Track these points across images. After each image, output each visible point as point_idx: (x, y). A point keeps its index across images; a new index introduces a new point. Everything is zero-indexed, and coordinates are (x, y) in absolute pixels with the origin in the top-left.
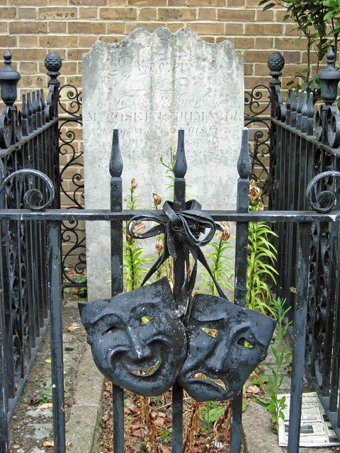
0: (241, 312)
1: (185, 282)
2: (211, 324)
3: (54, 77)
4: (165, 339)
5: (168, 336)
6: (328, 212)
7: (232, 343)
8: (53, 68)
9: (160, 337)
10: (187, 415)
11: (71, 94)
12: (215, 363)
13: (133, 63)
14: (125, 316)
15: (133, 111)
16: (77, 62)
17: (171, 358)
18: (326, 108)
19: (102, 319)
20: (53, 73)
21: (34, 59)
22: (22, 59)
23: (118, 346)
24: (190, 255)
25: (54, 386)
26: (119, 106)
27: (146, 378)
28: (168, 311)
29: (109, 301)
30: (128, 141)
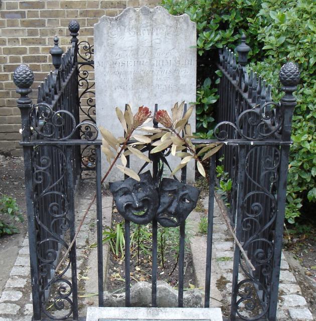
0: (184, 186)
1: (158, 172)
2: (170, 192)
3: (74, 37)
4: (149, 199)
5: (150, 197)
6: (224, 140)
7: (180, 200)
8: (74, 31)
9: (147, 198)
10: (159, 236)
11: (86, 47)
12: (172, 209)
13: (126, 30)
14: (131, 188)
15: (126, 61)
16: (86, 18)
17: (152, 207)
18: (241, 67)
19: (120, 189)
20: (74, 34)
21: (57, 17)
22: (49, 17)
23: (127, 202)
24: (161, 160)
25: (98, 220)
26: (118, 57)
27: (141, 216)
28: (151, 186)
29: (123, 181)
30: (123, 79)
